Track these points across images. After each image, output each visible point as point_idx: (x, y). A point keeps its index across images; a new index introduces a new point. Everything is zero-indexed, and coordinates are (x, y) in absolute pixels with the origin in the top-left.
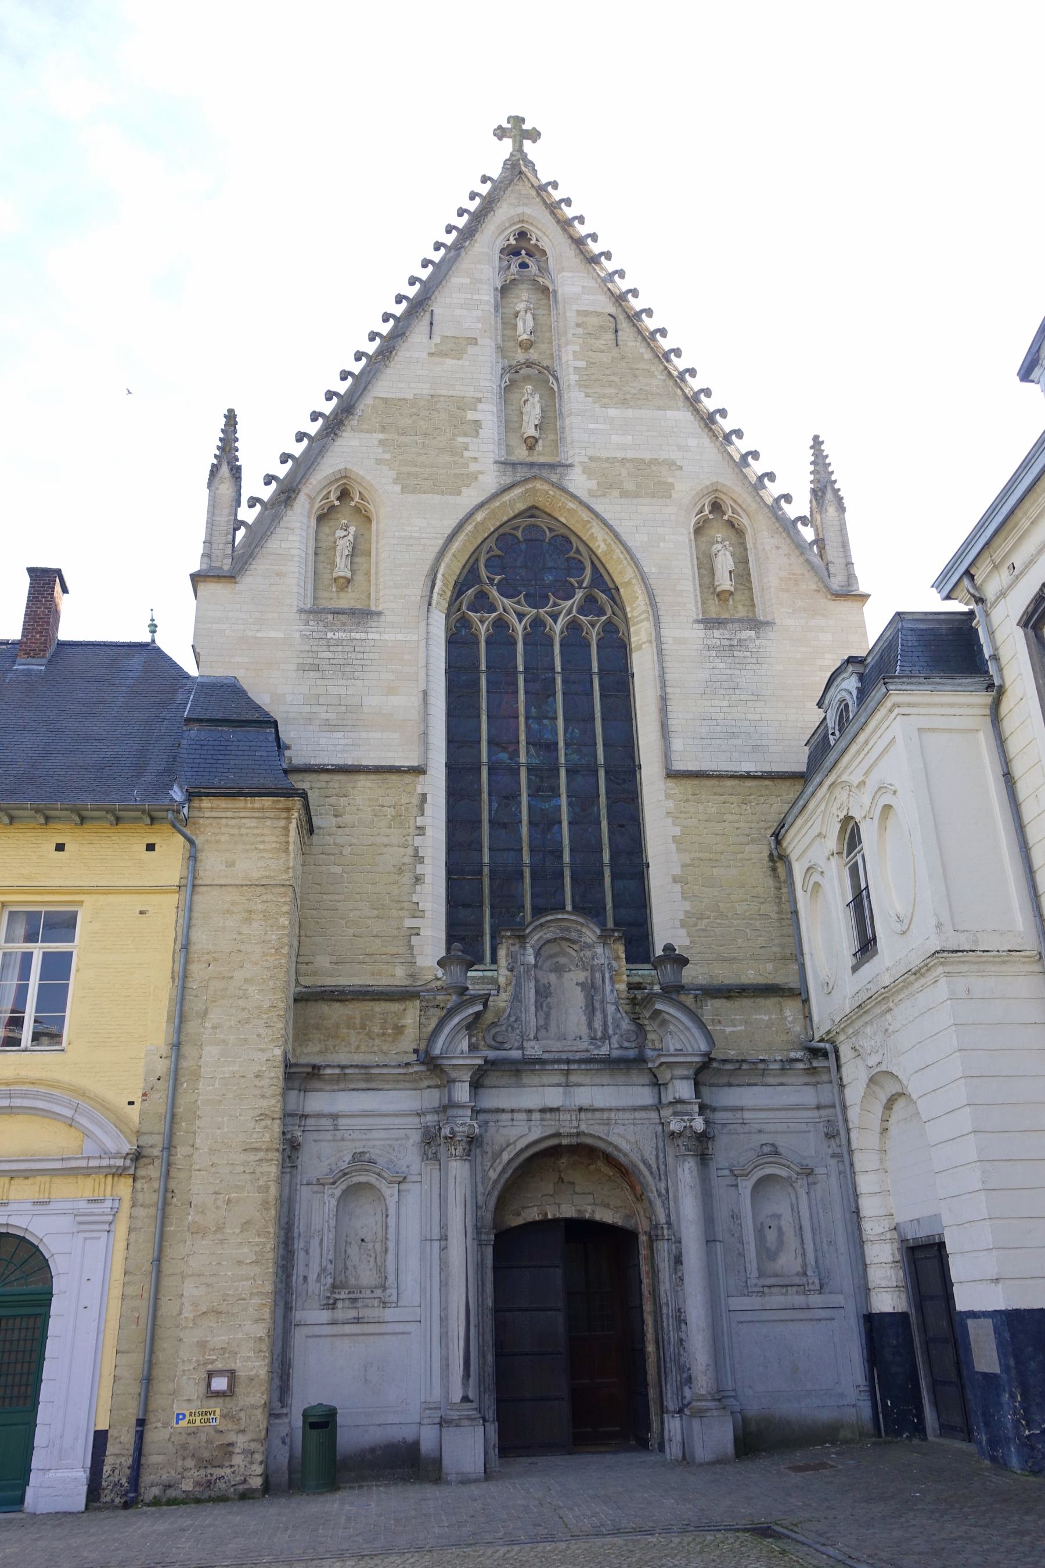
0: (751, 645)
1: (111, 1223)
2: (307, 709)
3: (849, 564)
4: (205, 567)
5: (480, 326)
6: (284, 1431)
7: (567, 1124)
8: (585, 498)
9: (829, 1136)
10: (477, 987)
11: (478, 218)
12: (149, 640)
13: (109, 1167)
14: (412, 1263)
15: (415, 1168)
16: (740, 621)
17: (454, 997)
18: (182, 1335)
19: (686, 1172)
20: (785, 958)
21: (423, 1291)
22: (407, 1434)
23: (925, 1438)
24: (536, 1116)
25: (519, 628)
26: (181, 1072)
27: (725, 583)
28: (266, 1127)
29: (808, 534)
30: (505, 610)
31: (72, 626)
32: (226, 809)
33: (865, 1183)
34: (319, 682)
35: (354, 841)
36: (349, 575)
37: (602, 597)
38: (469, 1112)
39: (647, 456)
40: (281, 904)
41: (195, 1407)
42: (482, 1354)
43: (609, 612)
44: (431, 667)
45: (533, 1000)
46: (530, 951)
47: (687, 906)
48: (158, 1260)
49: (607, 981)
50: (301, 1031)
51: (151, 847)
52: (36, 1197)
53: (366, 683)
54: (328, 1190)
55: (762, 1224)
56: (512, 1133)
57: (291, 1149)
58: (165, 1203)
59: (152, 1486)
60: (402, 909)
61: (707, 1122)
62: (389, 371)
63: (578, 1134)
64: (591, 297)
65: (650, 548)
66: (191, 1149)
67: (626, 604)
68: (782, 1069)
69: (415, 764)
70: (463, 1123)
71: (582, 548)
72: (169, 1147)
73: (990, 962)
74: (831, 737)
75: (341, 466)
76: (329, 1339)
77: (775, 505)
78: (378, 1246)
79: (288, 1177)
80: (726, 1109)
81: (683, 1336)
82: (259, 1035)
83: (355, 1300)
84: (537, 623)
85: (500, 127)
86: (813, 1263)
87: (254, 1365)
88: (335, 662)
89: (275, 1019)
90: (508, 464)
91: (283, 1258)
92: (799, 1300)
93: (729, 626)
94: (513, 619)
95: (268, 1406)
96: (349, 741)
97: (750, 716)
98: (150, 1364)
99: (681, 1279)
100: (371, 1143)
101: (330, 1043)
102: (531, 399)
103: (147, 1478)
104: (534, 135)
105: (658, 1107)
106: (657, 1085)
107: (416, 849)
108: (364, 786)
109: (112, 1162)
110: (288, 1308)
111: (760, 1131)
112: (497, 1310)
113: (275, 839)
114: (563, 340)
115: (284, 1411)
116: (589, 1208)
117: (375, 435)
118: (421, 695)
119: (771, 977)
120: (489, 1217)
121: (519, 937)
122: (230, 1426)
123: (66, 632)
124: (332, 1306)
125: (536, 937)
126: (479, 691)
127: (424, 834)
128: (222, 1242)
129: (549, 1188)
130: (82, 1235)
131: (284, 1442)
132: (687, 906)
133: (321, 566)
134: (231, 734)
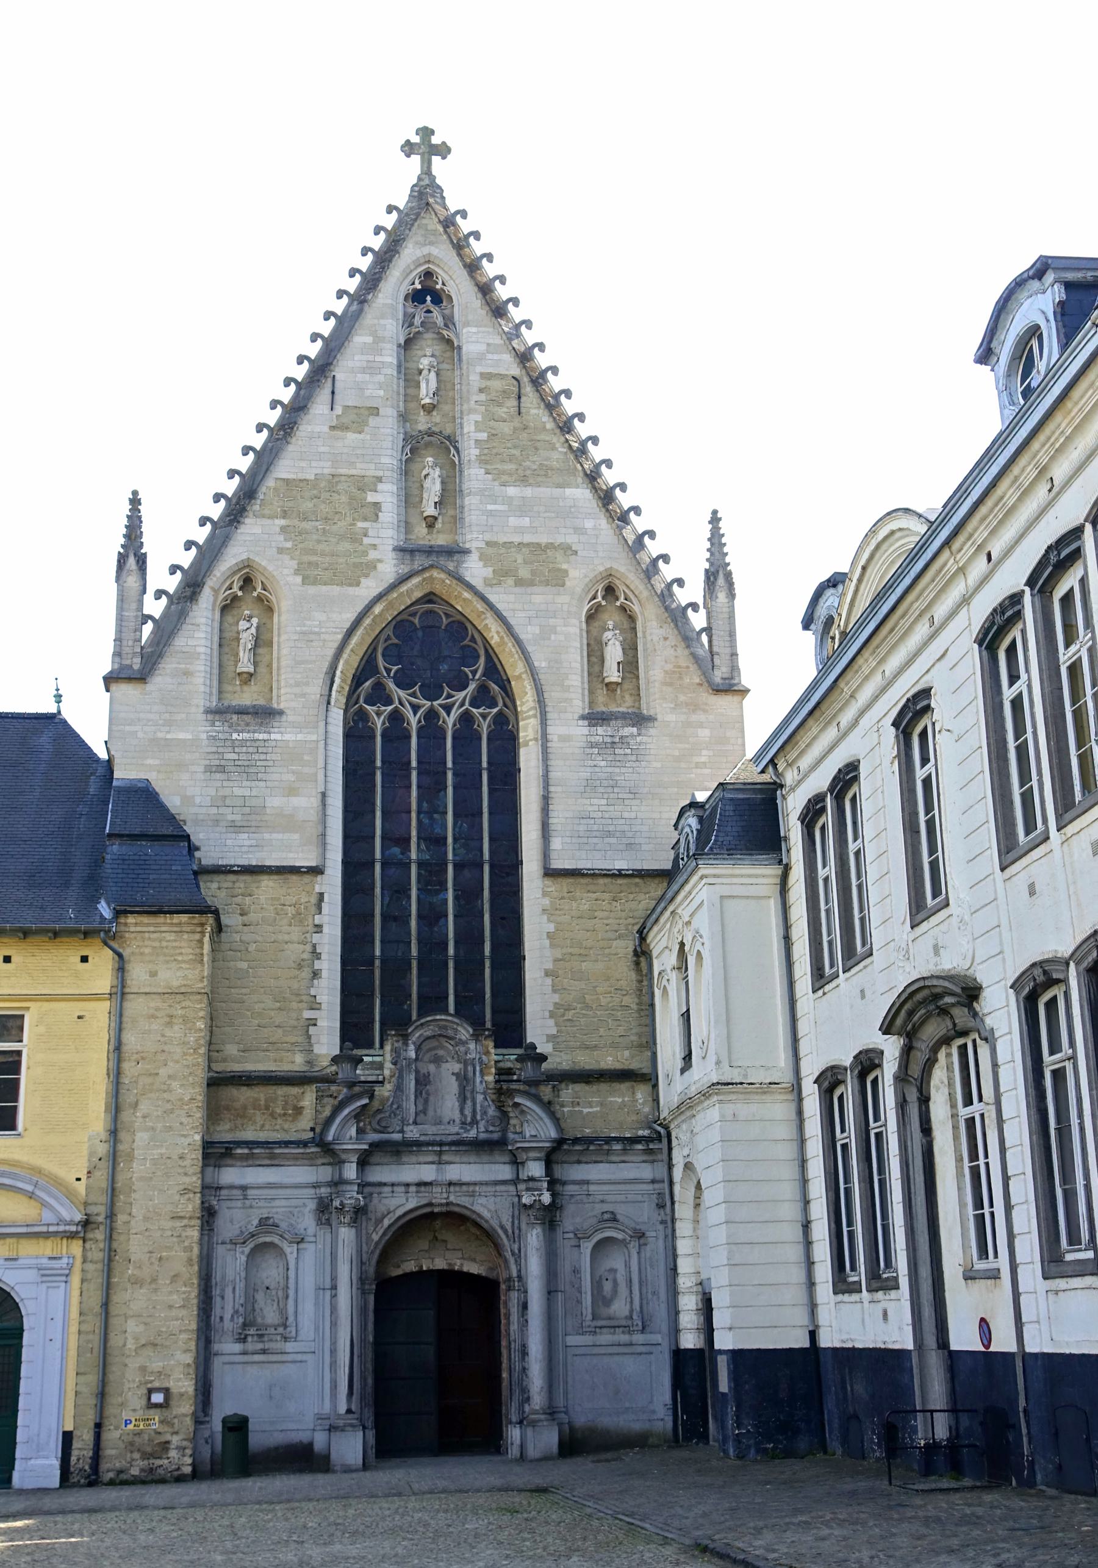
1: (67, 1276)
3: (734, 655)
4: (116, 666)
5: (381, 393)
6: (207, 1434)
7: (439, 1196)
9: (661, 1206)
10: (367, 1072)
12: (55, 711)
13: (65, 1232)
14: (308, 1309)
16: (624, 716)
17: (345, 1090)
18: (127, 1361)
19: (534, 1238)
21: (317, 1329)
22: (304, 1437)
23: (707, 1443)
24: (413, 1189)
25: (413, 721)
26: (118, 1154)
28: (189, 1199)
29: (698, 620)
30: (401, 703)
32: (148, 925)
33: (683, 1246)
34: (225, 784)
36: (252, 670)
37: (494, 687)
38: (356, 1188)
39: (543, 539)
40: (198, 1009)
41: (139, 1414)
42: (363, 1379)
43: (501, 704)
46: (412, 1047)
47: (556, 998)
48: (106, 1305)
49: (478, 1073)
50: (213, 1112)
51: (84, 959)
52: (7, 1255)
53: (269, 784)
54: (239, 1248)
55: (600, 1277)
56: (393, 1203)
57: (208, 1215)
58: (110, 1260)
59: (108, 1471)
60: (301, 1001)
62: (291, 448)
63: (447, 1204)
64: (496, 357)
65: (542, 638)
67: (516, 697)
68: (624, 1150)
69: (314, 864)
70: (352, 1196)
71: (476, 636)
72: (111, 1216)
74: (681, 862)
75: (244, 557)
76: (240, 1366)
77: (666, 593)
78: (280, 1293)
79: (206, 1238)
80: (574, 1182)
82: (181, 1123)
83: (262, 1336)
84: (431, 715)
85: (408, 142)
87: (184, 1385)
88: (240, 763)
89: (195, 1110)
90: (406, 551)
91: (204, 1302)
92: (624, 1338)
93: (613, 723)
94: (408, 712)
95: (194, 1414)
96: (254, 842)
97: (626, 815)
98: (104, 1383)
99: (527, 1321)
100: (274, 1210)
101: (239, 1121)
103: (104, 1466)
104: (443, 151)
105: (516, 1181)
106: (516, 1162)
107: (314, 946)
108: (267, 886)
109: (67, 1228)
111: (602, 1201)
112: (377, 1343)
113: (191, 951)
114: (465, 407)
115: (207, 1419)
116: (458, 1262)
118: (319, 796)
119: (627, 1063)
120: (371, 1270)
121: (402, 1035)
122: (166, 1429)
124: (243, 1340)
125: (417, 1035)
126: (374, 786)
128: (156, 1290)
129: (424, 1244)
130: (44, 1285)
131: (207, 1442)
132: (556, 998)
133: (225, 657)
134: (150, 849)
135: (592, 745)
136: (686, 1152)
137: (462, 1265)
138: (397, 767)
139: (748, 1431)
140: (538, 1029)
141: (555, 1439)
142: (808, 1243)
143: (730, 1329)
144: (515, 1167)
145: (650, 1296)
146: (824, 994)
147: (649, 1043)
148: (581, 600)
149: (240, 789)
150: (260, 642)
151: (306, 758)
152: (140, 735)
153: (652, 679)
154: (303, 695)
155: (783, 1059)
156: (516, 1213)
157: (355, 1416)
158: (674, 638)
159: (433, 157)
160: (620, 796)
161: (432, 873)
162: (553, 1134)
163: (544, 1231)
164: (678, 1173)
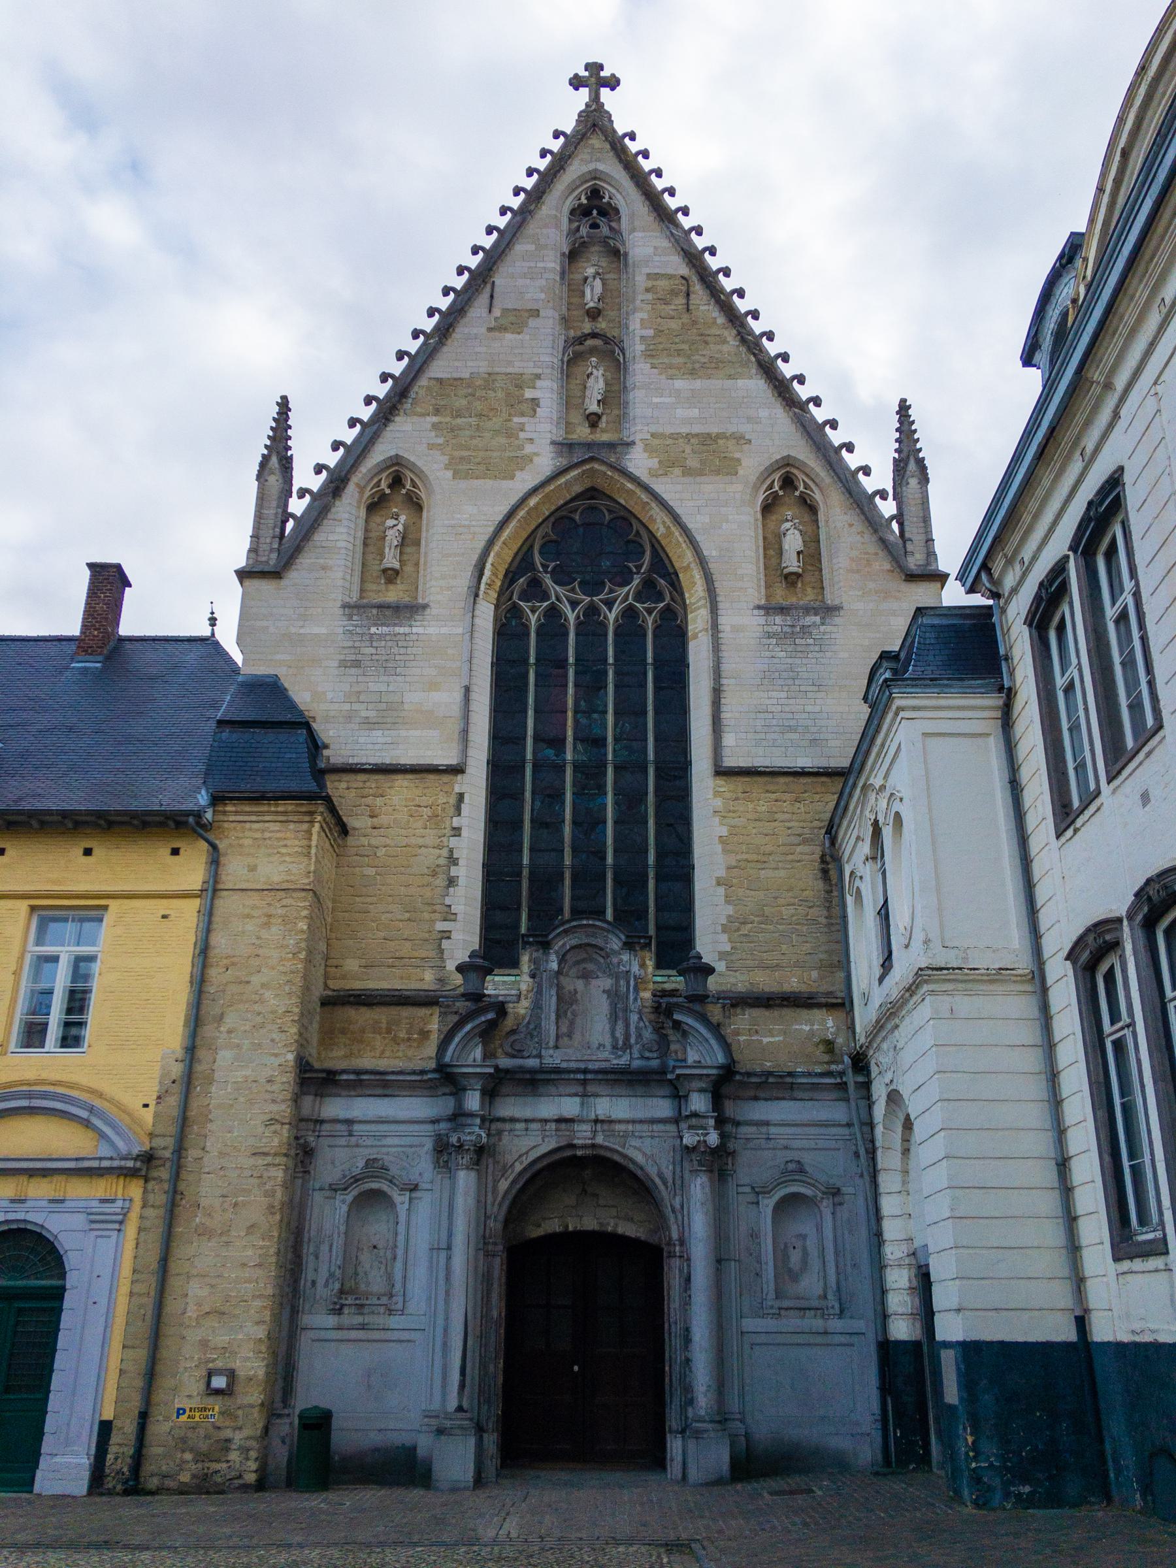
0: (815, 631)
1: (121, 1223)
2: (347, 707)
3: (930, 541)
7: (583, 1135)
8: (645, 477)
11: (547, 179)
13: (121, 1168)
15: (428, 1176)
19: (699, 1188)
20: (831, 966)
22: (405, 1439)
26: (194, 1076)
27: (792, 564)
28: (275, 1132)
29: (887, 508)
30: (558, 599)
31: (133, 621)
33: (889, 1205)
35: (388, 842)
36: (397, 565)
38: (478, 1121)
39: (714, 430)
43: (668, 598)
44: (475, 661)
45: (553, 1007)
46: (553, 957)
47: (730, 910)
53: (408, 679)
57: (302, 1155)
59: (152, 1475)
61: (723, 1136)
65: (717, 526)
66: (200, 1152)
70: (474, 1133)
72: (180, 1150)
73: (978, 981)
75: (393, 453)
81: (689, 1355)
83: (362, 1306)
84: (592, 610)
85: (576, 76)
86: (834, 1286)
87: (252, 1365)
90: (565, 446)
92: (818, 1324)
94: (566, 608)
96: (389, 740)
97: (809, 708)
100: (384, 1150)
102: (595, 371)
103: (148, 1468)
104: (613, 83)
105: (676, 1120)
106: (678, 1096)
107: (451, 851)
108: (401, 790)
109: (123, 1163)
110: (295, 1312)
111: (786, 1148)
115: (286, 1411)
117: (428, 419)
118: (463, 690)
123: (128, 626)
124: (338, 1311)
125: (560, 943)
126: (526, 684)
127: (459, 835)
129: (570, 1200)
131: (283, 1442)
132: (730, 910)
133: (370, 557)
135: (769, 635)
136: (888, 1077)
137: (617, 1225)
138: (553, 663)
139: (991, 1465)
140: (709, 940)
141: (726, 1458)
142: (1066, 1190)
143: (959, 1310)
144: (676, 1103)
145: (849, 1269)
146: (1076, 831)
147: (841, 962)
148: (756, 488)
149: (377, 684)
150: (407, 541)
151: (450, 651)
152: (272, 630)
153: (836, 567)
154: (449, 588)
155: (1016, 938)
156: (678, 1158)
157: (468, 1415)
158: (859, 525)
159: (602, 89)
160: (802, 688)
161: (589, 775)
162: (721, 1059)
163: (711, 1180)
164: (879, 1110)
